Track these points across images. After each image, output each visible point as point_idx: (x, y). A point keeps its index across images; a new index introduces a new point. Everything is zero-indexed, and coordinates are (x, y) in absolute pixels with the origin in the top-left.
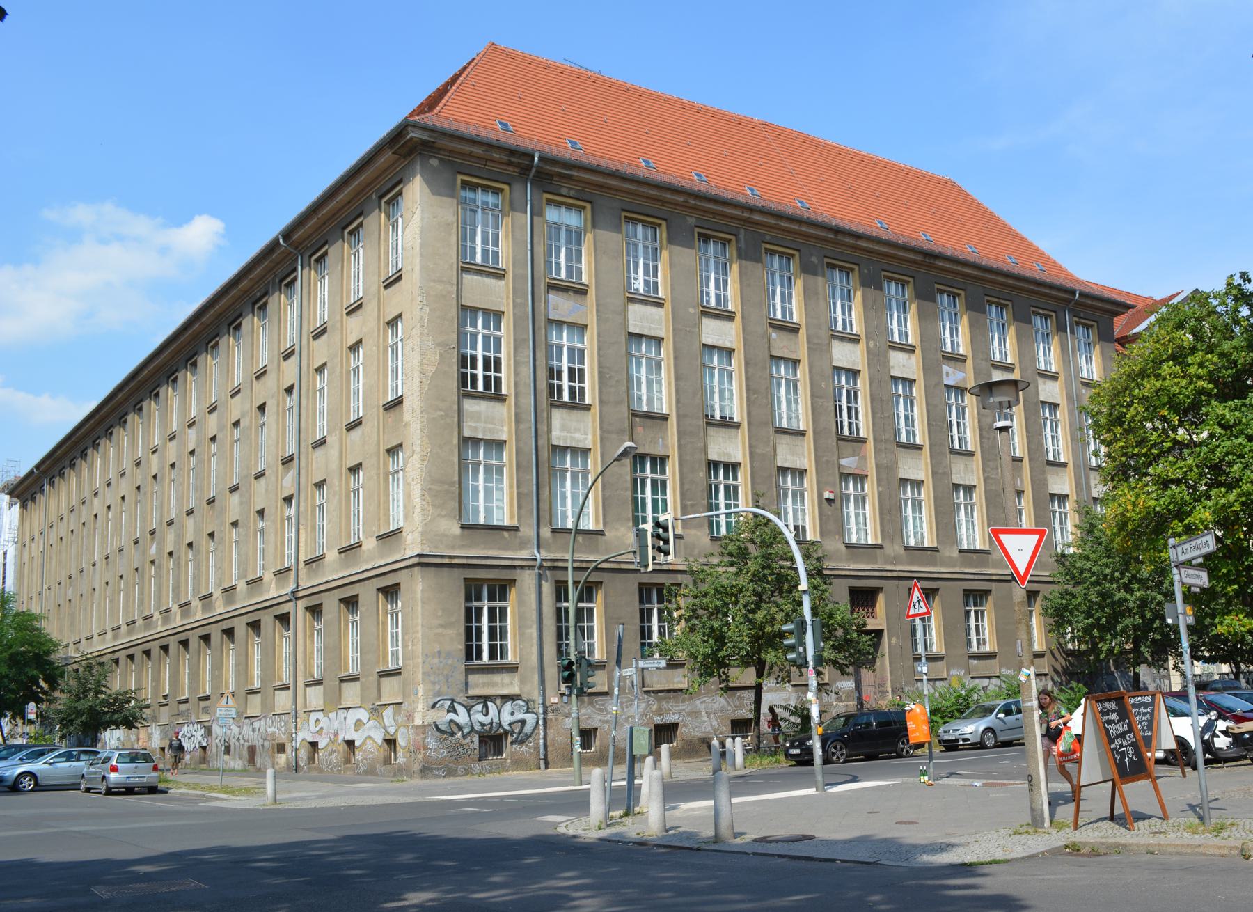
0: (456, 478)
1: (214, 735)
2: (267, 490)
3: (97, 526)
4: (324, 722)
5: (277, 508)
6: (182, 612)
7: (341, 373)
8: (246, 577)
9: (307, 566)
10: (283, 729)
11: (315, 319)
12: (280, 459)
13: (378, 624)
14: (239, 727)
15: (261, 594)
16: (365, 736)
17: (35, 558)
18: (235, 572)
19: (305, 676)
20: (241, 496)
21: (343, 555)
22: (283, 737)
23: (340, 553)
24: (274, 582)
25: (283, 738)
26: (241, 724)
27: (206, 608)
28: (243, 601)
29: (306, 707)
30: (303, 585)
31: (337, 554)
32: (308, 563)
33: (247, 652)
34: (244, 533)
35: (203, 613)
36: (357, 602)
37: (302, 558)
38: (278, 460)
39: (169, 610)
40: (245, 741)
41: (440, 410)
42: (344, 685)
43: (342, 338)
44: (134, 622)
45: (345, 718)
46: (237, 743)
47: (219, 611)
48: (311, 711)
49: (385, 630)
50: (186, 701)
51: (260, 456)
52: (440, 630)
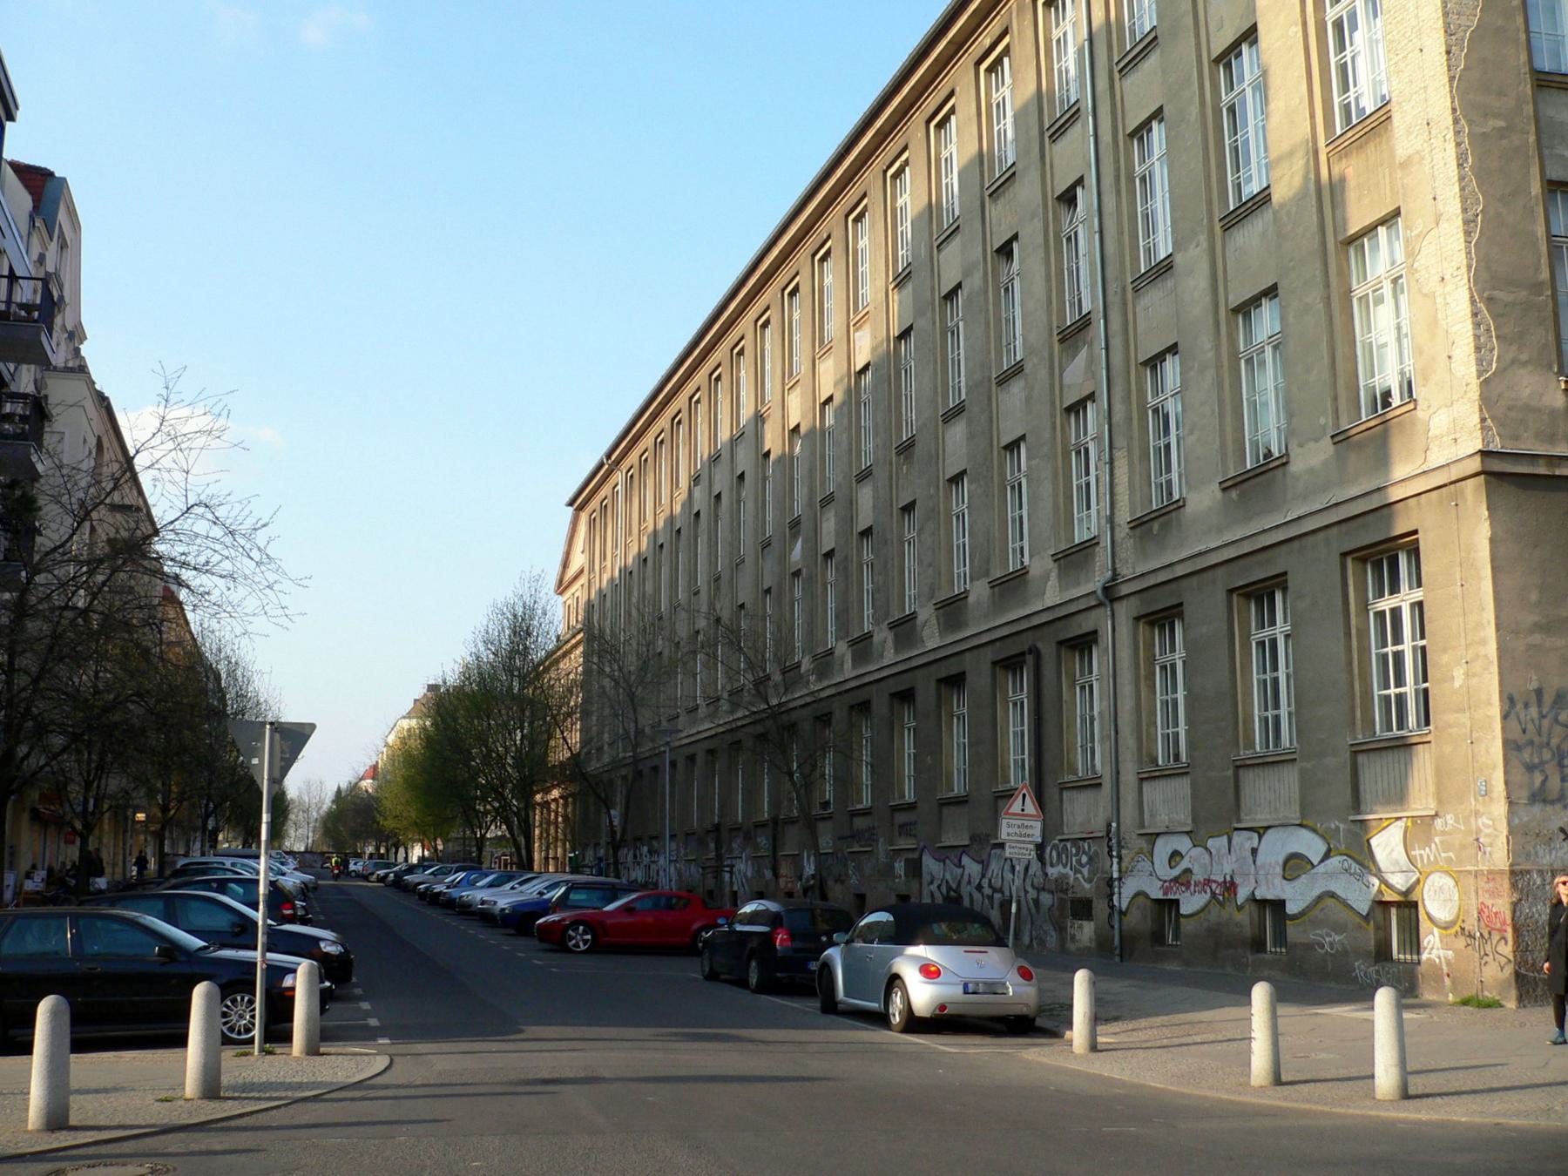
0: (1545, 275)
1: (926, 878)
2: (1028, 399)
3: (681, 546)
4: (1194, 858)
5: (1054, 428)
6: (896, 636)
7: (1203, 114)
8: (987, 574)
9: (1138, 531)
10: (1085, 871)
11: (992, 169)
12: (1055, 332)
13: (1348, 634)
14: (981, 862)
15: (1025, 603)
16: (1316, 893)
17: (724, 498)
18: (868, 612)
19: (1140, 761)
20: (970, 422)
21: (1234, 494)
22: (1087, 886)
23: (1224, 490)
24: (1054, 576)
25: (1086, 887)
26: (985, 857)
27: (900, 644)
28: (981, 623)
29: (1142, 825)
30: (1126, 571)
31: (1219, 494)
32: (1138, 524)
33: (995, 718)
34: (979, 491)
35: (897, 651)
36: (964, 680)
37: (1124, 516)
38: (1051, 335)
39: (830, 652)
40: (995, 890)
41: (1497, 116)
42: (945, 810)
43: (1198, 45)
44: (696, 708)
45: (1254, 851)
46: (976, 895)
47: (930, 645)
48: (1158, 834)
49: (1364, 650)
50: (866, 813)
51: (1004, 343)
52: (1537, 638)
